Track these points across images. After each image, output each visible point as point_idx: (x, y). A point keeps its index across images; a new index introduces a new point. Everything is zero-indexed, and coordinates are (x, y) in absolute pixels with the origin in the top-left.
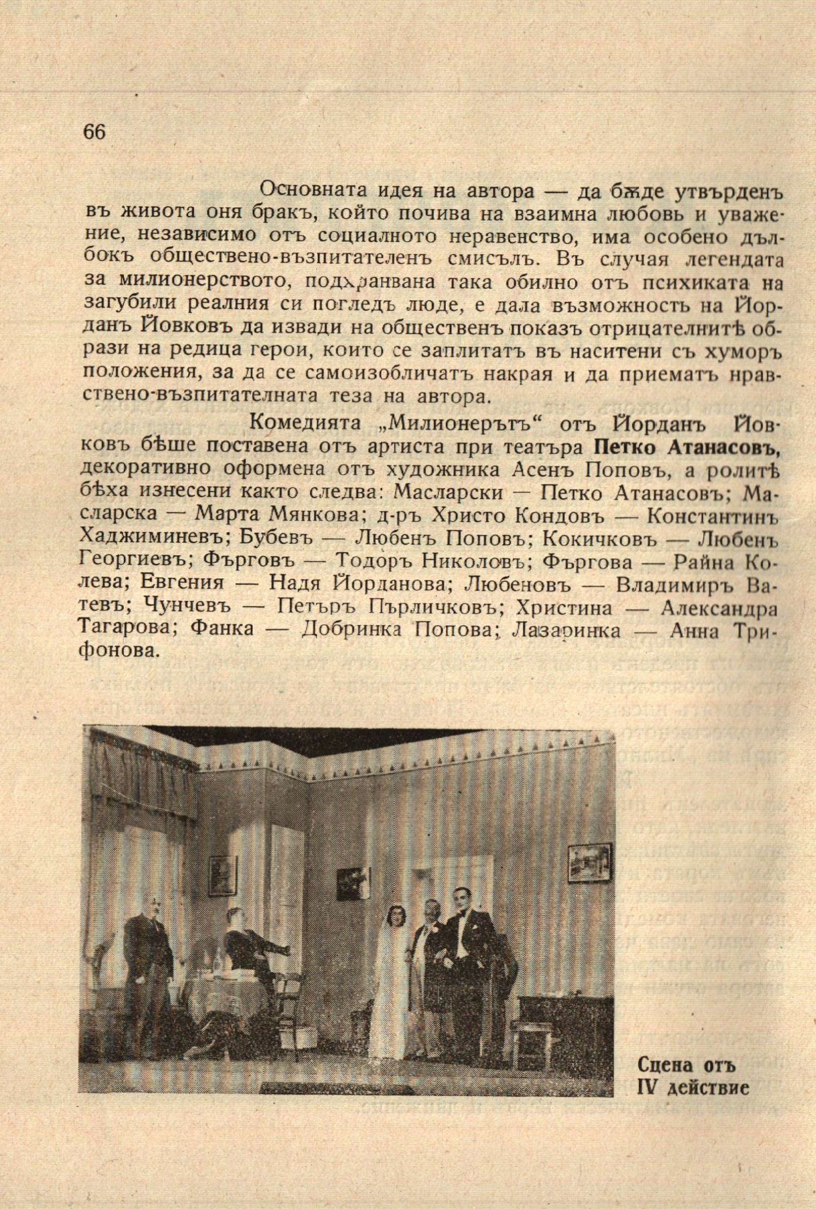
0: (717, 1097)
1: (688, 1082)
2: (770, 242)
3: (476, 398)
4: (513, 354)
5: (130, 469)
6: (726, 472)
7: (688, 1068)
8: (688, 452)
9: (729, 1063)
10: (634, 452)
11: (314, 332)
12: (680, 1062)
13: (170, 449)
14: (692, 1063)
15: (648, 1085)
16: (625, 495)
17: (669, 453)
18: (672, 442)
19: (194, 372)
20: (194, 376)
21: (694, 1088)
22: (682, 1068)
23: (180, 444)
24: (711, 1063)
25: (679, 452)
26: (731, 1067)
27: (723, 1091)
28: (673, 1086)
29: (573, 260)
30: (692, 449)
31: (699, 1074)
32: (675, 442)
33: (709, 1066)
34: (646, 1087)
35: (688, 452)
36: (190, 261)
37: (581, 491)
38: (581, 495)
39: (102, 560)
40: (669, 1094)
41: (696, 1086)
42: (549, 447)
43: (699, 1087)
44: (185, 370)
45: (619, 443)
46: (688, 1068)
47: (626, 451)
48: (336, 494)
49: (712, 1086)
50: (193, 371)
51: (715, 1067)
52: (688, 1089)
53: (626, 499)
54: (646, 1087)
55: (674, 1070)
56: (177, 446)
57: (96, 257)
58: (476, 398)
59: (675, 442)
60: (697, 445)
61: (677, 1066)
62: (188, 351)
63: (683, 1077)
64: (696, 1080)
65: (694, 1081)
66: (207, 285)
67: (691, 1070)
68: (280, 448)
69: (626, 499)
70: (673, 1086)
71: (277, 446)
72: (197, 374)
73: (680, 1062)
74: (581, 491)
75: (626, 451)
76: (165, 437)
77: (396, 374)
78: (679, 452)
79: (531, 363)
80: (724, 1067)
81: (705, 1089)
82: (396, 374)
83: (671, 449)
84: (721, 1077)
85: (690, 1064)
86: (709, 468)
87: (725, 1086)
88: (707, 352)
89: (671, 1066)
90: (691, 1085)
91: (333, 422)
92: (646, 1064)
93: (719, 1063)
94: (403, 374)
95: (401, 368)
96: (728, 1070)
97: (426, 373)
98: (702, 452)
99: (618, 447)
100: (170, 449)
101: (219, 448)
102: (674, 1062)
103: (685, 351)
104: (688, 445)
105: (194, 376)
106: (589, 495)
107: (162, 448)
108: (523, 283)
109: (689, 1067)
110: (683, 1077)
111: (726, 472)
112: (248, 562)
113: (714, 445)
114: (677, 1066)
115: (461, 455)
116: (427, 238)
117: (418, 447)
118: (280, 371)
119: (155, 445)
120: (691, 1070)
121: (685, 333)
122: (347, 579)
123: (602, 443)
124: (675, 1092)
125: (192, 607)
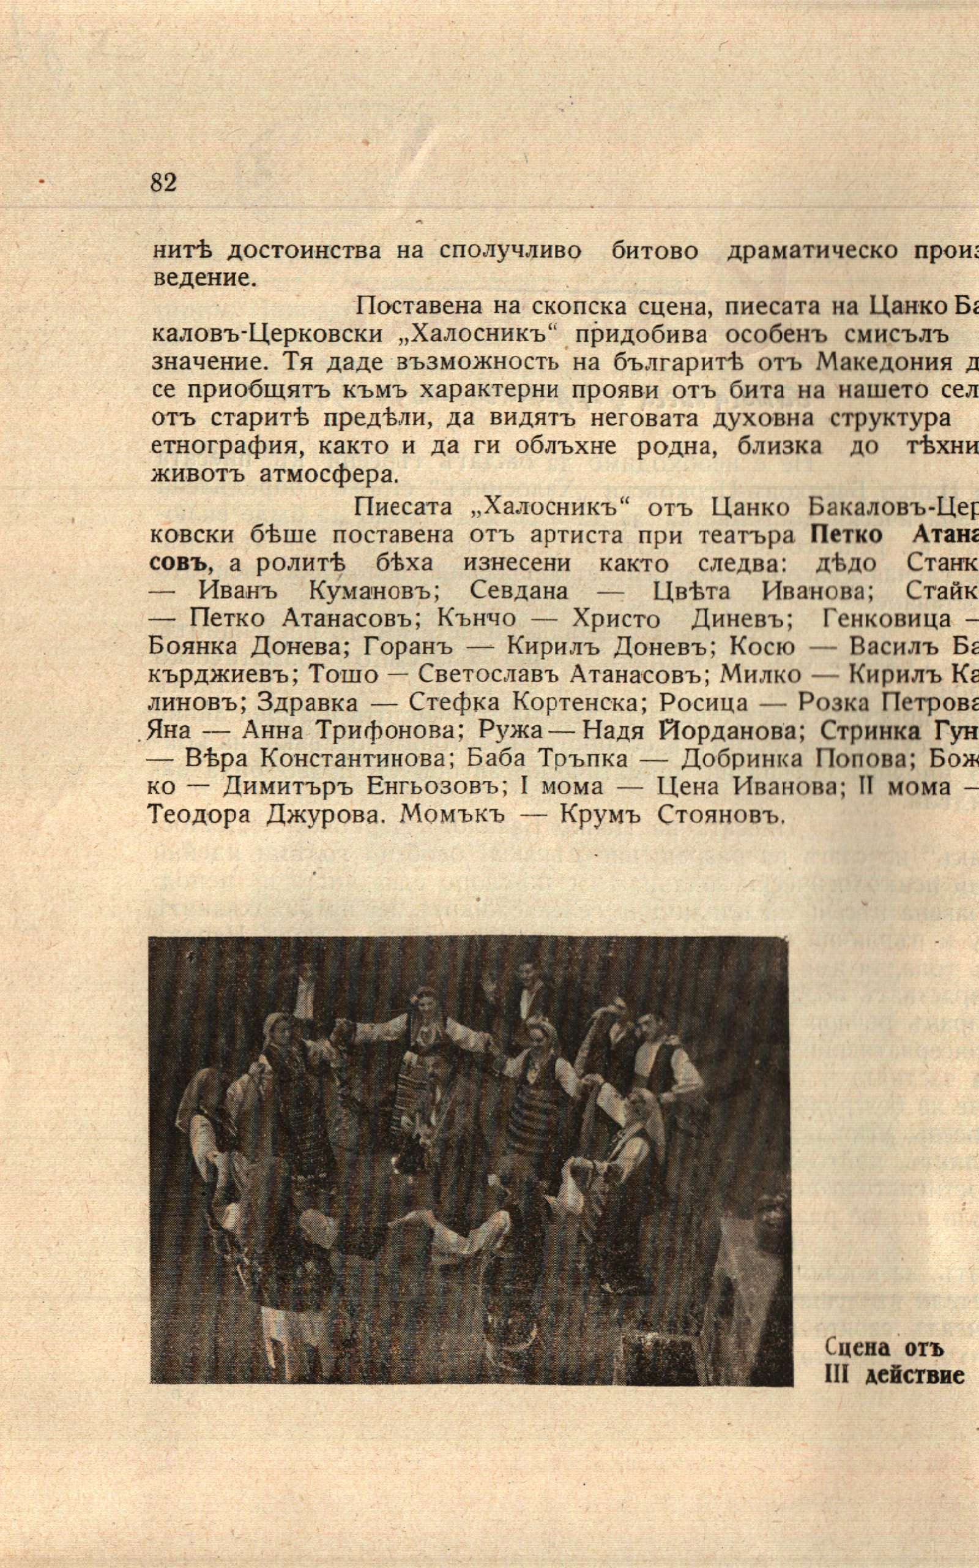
0: (926, 1387)
1: (889, 1368)
2: (647, 369)
3: (381, 476)
4: (560, 420)
5: (227, 816)
6: (279, 564)
7: (884, 1351)
8: (937, 540)
9: (936, 1346)
10: (858, 541)
11: (612, 737)
12: (874, 1344)
13: (286, 541)
14: (890, 1346)
15: (501, 250)
16: (294, 620)
17: (915, 541)
18: (917, 528)
19: (294, 447)
20: (294, 452)
21: (897, 1376)
22: (877, 1351)
23: (297, 534)
24: (914, 1345)
25: (926, 540)
26: (938, 1351)
27: (933, 1379)
28: (871, 1372)
29: (630, 364)
30: (942, 536)
31: (898, 1357)
32: (922, 528)
33: (911, 1349)
34: (835, 1374)
35: (937, 540)
36: (661, 313)
37: (239, 615)
38: (239, 620)
39: (175, 817)
40: (868, 1382)
41: (899, 1372)
42: (754, 535)
43: (902, 1374)
44: (283, 445)
45: (841, 530)
46: (884, 1351)
47: (848, 540)
48: (730, 567)
49: (920, 1373)
50: (292, 447)
51: (919, 1349)
52: (889, 1377)
53: (296, 625)
54: (835, 1374)
55: (867, 1353)
56: (294, 536)
57: (650, 338)
58: (381, 476)
59: (922, 528)
60: (947, 531)
61: (871, 1349)
62: (360, 421)
63: (879, 1363)
64: (899, 1366)
65: (896, 1367)
66: (283, 341)
67: (887, 1354)
68: (420, 538)
69: (296, 625)
70: (871, 1372)
71: (416, 535)
72: (298, 450)
73: (874, 1344)
74: (239, 615)
75: (848, 540)
76: (280, 528)
77: (537, 446)
78: (926, 540)
79: (585, 431)
80: (929, 1350)
81: (910, 1376)
82: (537, 446)
83: (917, 536)
84: (929, 1362)
85: (887, 1346)
86: (259, 560)
87: (936, 1372)
88: (422, 391)
89: (864, 1349)
90: (893, 1372)
91: (294, 388)
92: (834, 1346)
93: (922, 1345)
94: (546, 446)
95: (543, 439)
96: (935, 1354)
97: (831, 250)
98: (953, 541)
99: (839, 534)
100: (286, 541)
101: (466, 253)
102: (867, 1344)
103: (905, 333)
104: (937, 532)
105: (294, 452)
106: (248, 620)
107: (275, 538)
108: (658, 335)
109: (885, 1350)
110: (879, 1363)
111: (279, 564)
112: (207, 448)
113: (968, 531)
114: (871, 1349)
115: (646, 546)
116: (286, 252)
117: (592, 536)
118: (538, 304)
119: (267, 536)
120: (887, 1354)
121: (967, 395)
122: (676, 726)
123: (819, 530)
124: (874, 1381)
125: (203, 363)
